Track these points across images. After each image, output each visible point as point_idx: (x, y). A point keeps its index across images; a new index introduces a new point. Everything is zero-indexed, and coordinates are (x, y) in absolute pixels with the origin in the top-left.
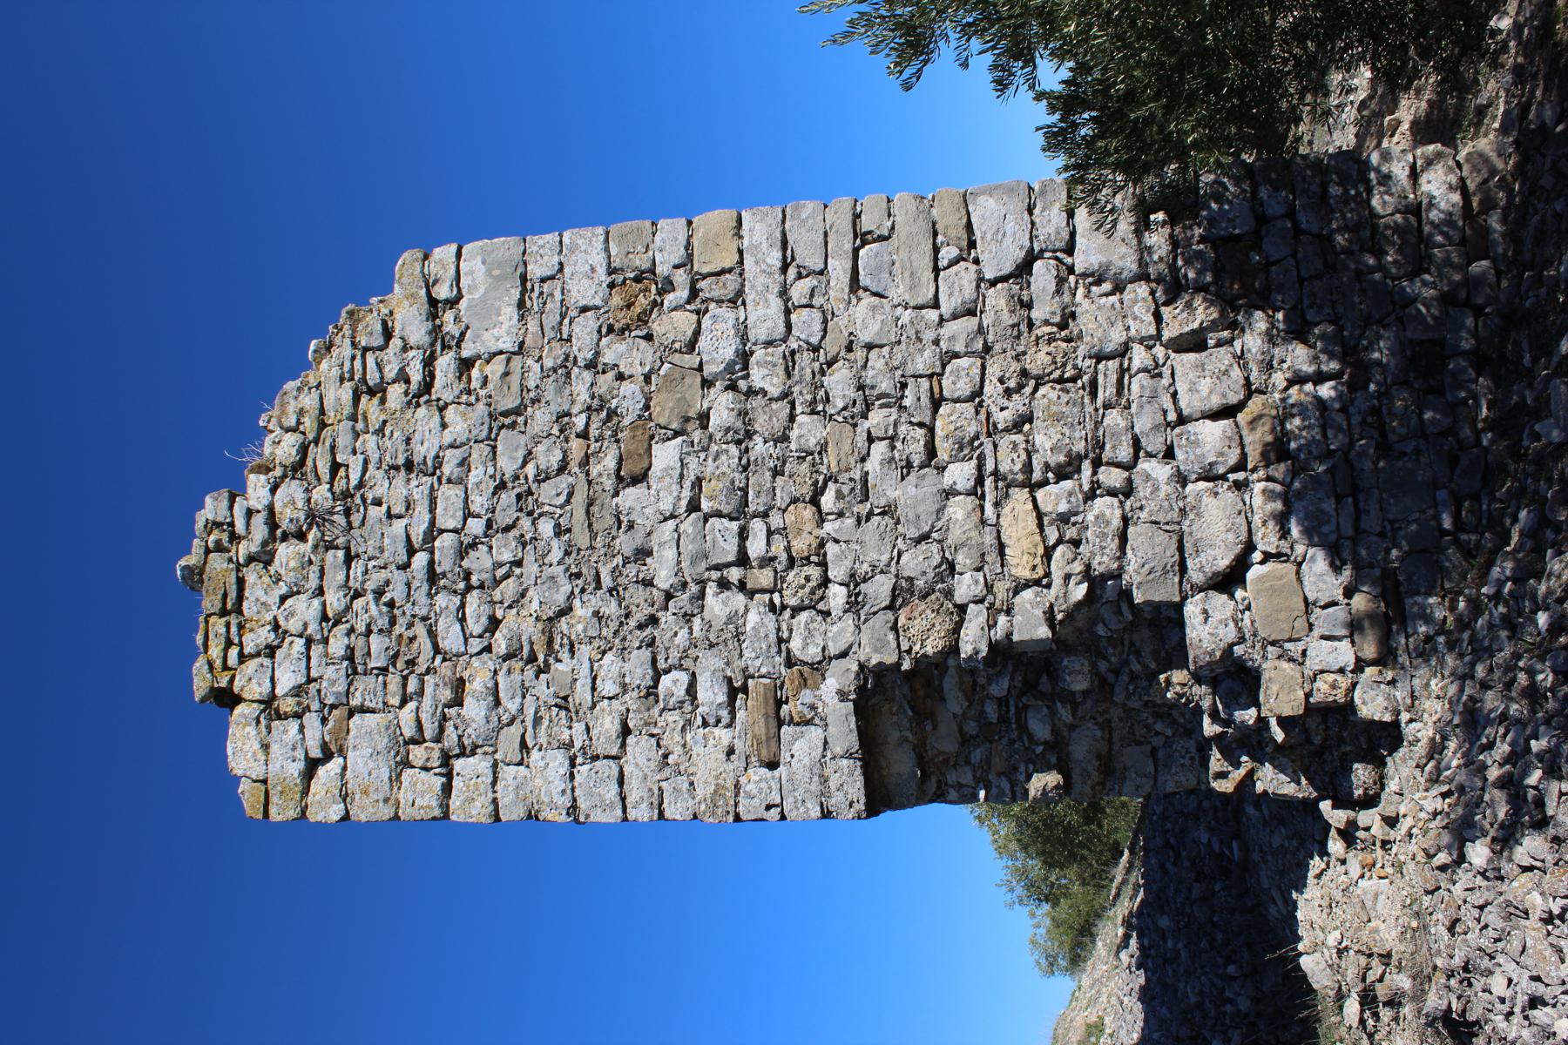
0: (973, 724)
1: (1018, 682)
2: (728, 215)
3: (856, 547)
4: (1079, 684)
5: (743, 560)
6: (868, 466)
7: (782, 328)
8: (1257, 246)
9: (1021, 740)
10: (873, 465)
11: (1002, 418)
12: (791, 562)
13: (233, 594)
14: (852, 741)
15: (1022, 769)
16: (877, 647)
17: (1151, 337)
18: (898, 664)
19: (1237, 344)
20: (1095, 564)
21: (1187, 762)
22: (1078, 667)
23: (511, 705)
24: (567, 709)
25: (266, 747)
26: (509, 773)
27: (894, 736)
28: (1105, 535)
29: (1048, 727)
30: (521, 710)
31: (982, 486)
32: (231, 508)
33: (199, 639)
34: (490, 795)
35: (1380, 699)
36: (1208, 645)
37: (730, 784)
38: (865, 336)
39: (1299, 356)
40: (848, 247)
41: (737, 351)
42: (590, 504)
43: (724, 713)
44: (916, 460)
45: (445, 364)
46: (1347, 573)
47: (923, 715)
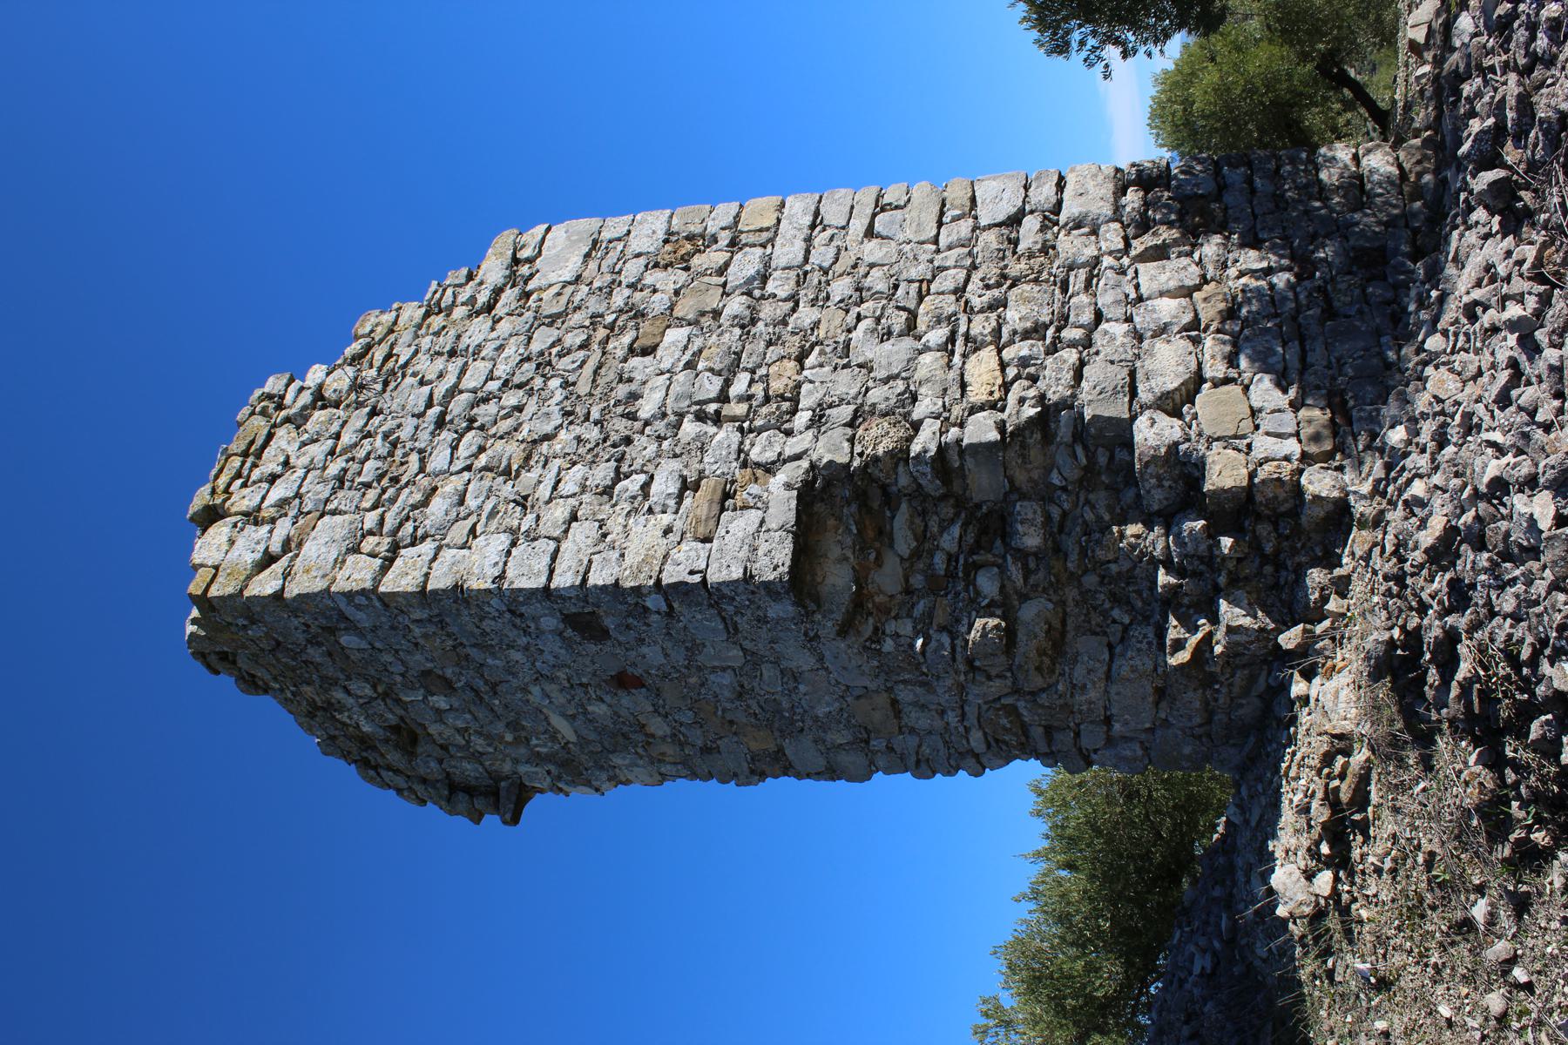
0: (920, 577)
1: (970, 538)
2: (776, 200)
3: (824, 382)
4: (1032, 539)
5: (723, 397)
6: (853, 335)
7: (800, 258)
8: (1218, 198)
9: (967, 590)
10: (857, 335)
11: (977, 302)
12: (767, 399)
13: (259, 442)
14: (791, 517)
15: (965, 621)
16: (832, 448)
17: (1119, 251)
18: (848, 465)
19: (1196, 256)
20: (1050, 395)
21: (1144, 646)
22: (1030, 516)
23: (472, 503)
24: (524, 507)
25: (232, 542)
26: (447, 555)
27: (836, 552)
28: (1061, 370)
29: (997, 584)
30: (480, 507)
31: (953, 345)
32: (288, 385)
33: (214, 472)
34: (425, 570)
35: (1328, 480)
36: (1152, 442)
37: (660, 555)
38: (869, 259)
39: (1251, 259)
40: (869, 211)
41: (758, 272)
42: (600, 367)
43: (672, 503)
44: (896, 329)
45: (509, 295)
46: (1292, 392)
47: (872, 539)
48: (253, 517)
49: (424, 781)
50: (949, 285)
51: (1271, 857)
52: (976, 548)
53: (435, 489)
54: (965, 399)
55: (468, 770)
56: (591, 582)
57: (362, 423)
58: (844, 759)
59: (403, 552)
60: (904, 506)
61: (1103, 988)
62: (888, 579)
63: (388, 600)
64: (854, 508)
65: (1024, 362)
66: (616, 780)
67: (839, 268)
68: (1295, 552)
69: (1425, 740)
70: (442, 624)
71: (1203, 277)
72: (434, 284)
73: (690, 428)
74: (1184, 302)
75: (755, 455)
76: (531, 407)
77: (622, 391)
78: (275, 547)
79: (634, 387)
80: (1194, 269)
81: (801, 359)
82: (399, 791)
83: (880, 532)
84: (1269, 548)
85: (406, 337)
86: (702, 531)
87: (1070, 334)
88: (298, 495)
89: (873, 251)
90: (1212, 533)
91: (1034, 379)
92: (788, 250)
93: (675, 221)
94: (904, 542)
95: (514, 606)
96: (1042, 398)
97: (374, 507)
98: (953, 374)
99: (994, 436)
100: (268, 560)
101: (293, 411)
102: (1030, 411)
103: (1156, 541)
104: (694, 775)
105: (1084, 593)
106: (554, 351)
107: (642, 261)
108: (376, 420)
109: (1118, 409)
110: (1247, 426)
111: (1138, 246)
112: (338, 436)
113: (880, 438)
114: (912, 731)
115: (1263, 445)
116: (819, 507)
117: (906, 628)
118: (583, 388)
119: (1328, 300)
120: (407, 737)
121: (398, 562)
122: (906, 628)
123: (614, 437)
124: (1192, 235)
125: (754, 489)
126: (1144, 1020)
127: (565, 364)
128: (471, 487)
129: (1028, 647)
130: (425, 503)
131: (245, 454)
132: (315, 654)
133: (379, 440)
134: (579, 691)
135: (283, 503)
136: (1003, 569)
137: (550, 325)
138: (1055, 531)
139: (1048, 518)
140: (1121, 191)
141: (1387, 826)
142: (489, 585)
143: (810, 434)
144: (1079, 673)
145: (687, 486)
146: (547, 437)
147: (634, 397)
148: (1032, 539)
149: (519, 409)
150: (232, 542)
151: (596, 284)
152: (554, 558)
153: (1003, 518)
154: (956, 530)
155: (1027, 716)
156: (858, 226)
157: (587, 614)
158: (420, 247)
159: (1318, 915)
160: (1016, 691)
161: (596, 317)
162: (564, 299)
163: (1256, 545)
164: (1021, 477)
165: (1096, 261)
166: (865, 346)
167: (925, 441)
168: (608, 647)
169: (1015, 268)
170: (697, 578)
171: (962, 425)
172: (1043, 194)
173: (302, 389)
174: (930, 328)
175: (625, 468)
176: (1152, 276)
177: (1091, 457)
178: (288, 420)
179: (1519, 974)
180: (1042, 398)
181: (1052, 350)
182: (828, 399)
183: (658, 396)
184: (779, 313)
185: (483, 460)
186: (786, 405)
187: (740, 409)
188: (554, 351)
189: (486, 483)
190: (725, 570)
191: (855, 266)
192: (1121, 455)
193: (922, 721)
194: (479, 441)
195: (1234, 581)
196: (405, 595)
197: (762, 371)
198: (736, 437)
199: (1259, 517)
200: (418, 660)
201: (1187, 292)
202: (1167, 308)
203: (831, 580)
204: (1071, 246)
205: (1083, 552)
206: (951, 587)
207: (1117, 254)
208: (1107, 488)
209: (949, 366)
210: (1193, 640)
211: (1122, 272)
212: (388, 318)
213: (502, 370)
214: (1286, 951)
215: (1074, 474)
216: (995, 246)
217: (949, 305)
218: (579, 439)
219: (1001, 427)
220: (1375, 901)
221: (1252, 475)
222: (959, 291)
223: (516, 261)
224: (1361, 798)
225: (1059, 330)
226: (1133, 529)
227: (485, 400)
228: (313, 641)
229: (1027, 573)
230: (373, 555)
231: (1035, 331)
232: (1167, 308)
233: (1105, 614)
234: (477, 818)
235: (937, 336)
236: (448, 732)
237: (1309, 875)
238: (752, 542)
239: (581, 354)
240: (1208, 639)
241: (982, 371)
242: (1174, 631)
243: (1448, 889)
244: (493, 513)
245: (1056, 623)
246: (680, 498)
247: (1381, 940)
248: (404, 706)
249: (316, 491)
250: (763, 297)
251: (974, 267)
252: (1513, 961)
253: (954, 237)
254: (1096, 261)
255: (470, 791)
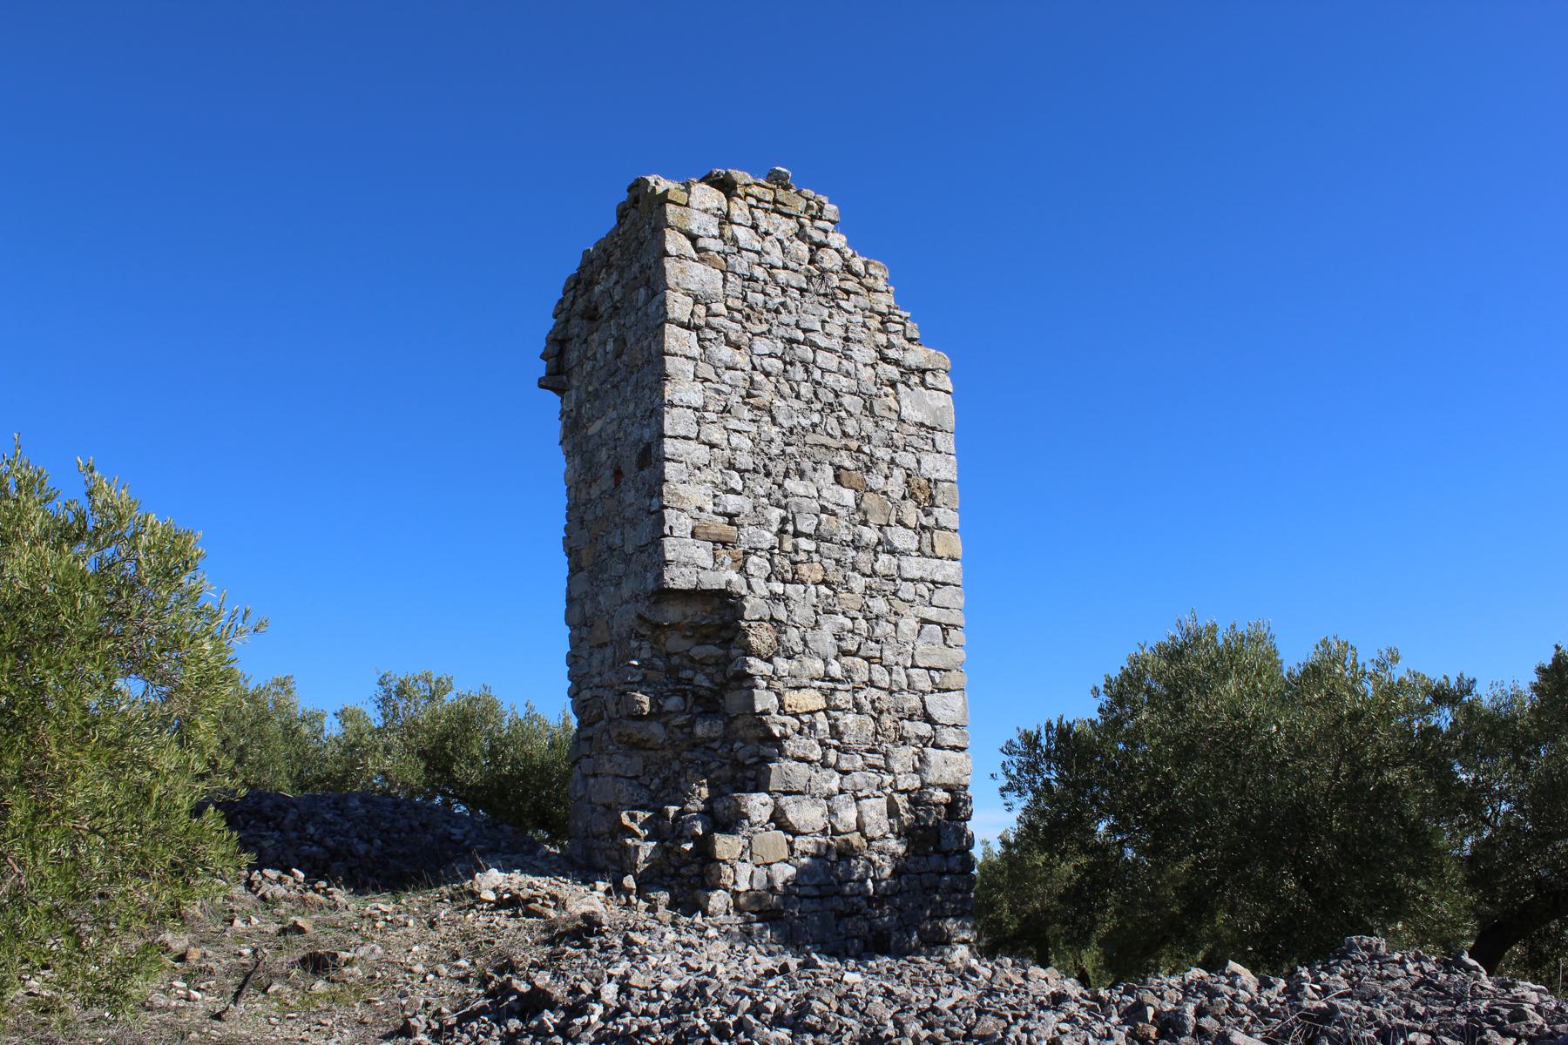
2: (959, 553)
3: (803, 601)
4: (700, 730)
5: (797, 534)
8: (936, 851)
10: (840, 618)
11: (861, 695)
12: (794, 563)
13: (785, 210)
14: (707, 586)
16: (754, 607)
23: (727, 376)
26: (690, 366)
27: (690, 611)
33: (762, 181)
37: (684, 506)
38: (901, 623)
43: (721, 509)
44: (843, 644)
45: (893, 372)
47: (701, 634)
48: (726, 219)
49: (567, 321)
50: (876, 677)
51: (510, 871)
52: (697, 697)
53: (739, 348)
54: (785, 692)
55: (573, 355)
56: (667, 464)
57: (794, 283)
58: (577, 609)
59: (694, 334)
60: (721, 652)
61: (461, 770)
62: (674, 643)
63: (661, 327)
64: (718, 622)
65: (812, 726)
66: (567, 454)
67: (896, 602)
68: (681, 886)
69: (550, 942)
70: (648, 362)
71: (873, 839)
72: (905, 314)
73: (775, 514)
74: (854, 826)
75: (753, 559)
76: (797, 404)
77: (807, 465)
78: (701, 243)
79: (809, 473)
80: (879, 833)
81: (824, 582)
82: (561, 301)
83: (707, 637)
84: (683, 871)
85: (863, 302)
86: (699, 531)
87: (832, 756)
88: (740, 250)
89: (909, 625)
90: (694, 838)
91: (800, 732)
92: (912, 567)
93: (946, 485)
94: (698, 652)
95: (655, 412)
96: (787, 737)
97: (728, 308)
98: (805, 681)
99: (759, 708)
100: (693, 239)
101: (808, 229)
102: (776, 731)
103: (695, 805)
104: (569, 509)
105: (669, 762)
106: (843, 414)
107: (914, 465)
108: (796, 294)
109: (775, 783)
110: (759, 860)
111: (901, 800)
112: (785, 268)
113: (761, 638)
114: (591, 654)
115: (745, 870)
116: (717, 601)
117: (645, 654)
118: (810, 438)
119: (849, 915)
120: (591, 315)
121: (686, 332)
122: (645, 654)
123: (771, 465)
124: (905, 833)
125: (728, 561)
126: (438, 800)
127: (832, 422)
128: (739, 373)
129: (633, 728)
130: (729, 343)
131: (775, 201)
132: (636, 268)
133: (778, 300)
134: (612, 444)
135: (735, 240)
136: (682, 712)
137: (865, 407)
138: (704, 745)
139: (714, 740)
140: (947, 788)
141: (512, 924)
142: (667, 397)
143: (766, 593)
144: (619, 758)
145: (731, 518)
146: (774, 421)
147: (802, 474)
148: (700, 730)
149: (798, 397)
150: (706, 211)
151: (895, 435)
152: (685, 438)
153: (716, 712)
154: (706, 684)
155: (597, 726)
156: (931, 613)
157: (651, 457)
158: (931, 302)
159: (473, 894)
160: (611, 720)
161: (868, 439)
162: (886, 413)
163: (686, 864)
164: (739, 723)
165: (890, 771)
166: (829, 625)
167: (757, 666)
168: (634, 469)
169: (887, 721)
170: (667, 531)
171: (768, 688)
172: (949, 737)
173: (826, 231)
174: (843, 666)
175: (747, 475)
176: (875, 811)
177: (750, 767)
178: (802, 226)
179: (430, 977)
180: (787, 737)
181: (822, 743)
182: (791, 604)
183: (801, 491)
184: (861, 566)
185: (758, 377)
186: (789, 576)
187: (788, 546)
188: (843, 414)
189: (741, 383)
190: (671, 548)
191: (896, 613)
192: (750, 785)
193: (595, 662)
194: (775, 371)
195: (667, 851)
196: (663, 342)
197: (816, 557)
198: (766, 546)
199: (702, 865)
200: (631, 340)
201: (860, 827)
202: (848, 816)
203: (671, 610)
204: (904, 757)
205: (692, 761)
206: (668, 679)
207: (894, 785)
208: (734, 777)
209: (812, 679)
210: (636, 827)
211: (880, 787)
212: (881, 285)
213: (830, 379)
214: (456, 879)
215: (740, 756)
216: (907, 706)
217: (861, 676)
218: (772, 440)
219: (766, 712)
220: (476, 920)
221: (724, 862)
222: (871, 683)
223: (924, 371)
224: (529, 913)
225: (836, 748)
226: (705, 792)
227: (807, 371)
228: (642, 270)
229: (681, 727)
230: (692, 313)
231: (835, 731)
232: (848, 816)
233: (656, 774)
234: (544, 356)
235: (836, 670)
236: (594, 345)
237: (495, 890)
238: (690, 563)
239: (838, 433)
240: (635, 835)
241: (811, 699)
242: (642, 815)
243: (476, 951)
244: (718, 392)
245: (649, 745)
246: (724, 514)
247: (454, 923)
248: (608, 321)
249: (741, 264)
250: (876, 553)
251: (891, 693)
252: (437, 974)
253: (916, 678)
254: (890, 771)
255: (561, 354)
